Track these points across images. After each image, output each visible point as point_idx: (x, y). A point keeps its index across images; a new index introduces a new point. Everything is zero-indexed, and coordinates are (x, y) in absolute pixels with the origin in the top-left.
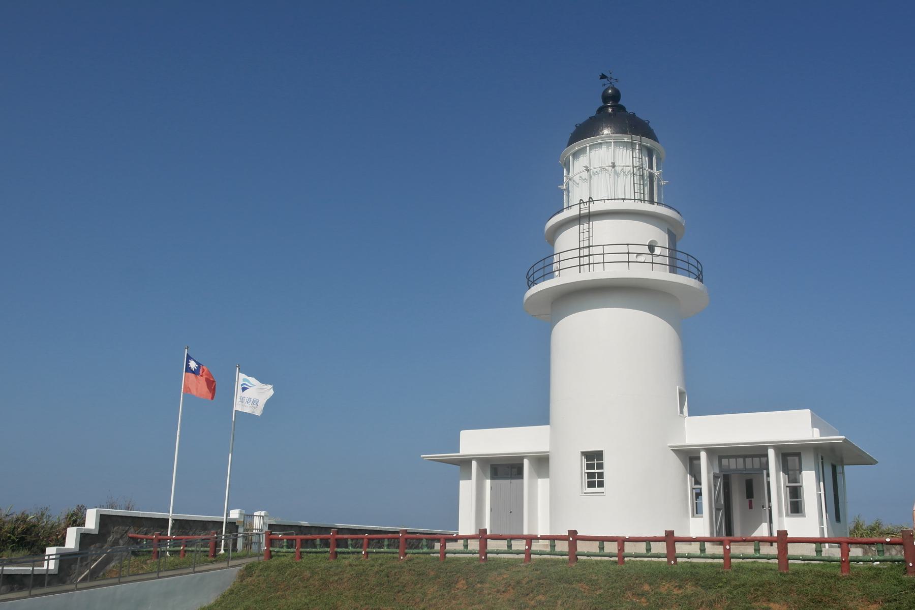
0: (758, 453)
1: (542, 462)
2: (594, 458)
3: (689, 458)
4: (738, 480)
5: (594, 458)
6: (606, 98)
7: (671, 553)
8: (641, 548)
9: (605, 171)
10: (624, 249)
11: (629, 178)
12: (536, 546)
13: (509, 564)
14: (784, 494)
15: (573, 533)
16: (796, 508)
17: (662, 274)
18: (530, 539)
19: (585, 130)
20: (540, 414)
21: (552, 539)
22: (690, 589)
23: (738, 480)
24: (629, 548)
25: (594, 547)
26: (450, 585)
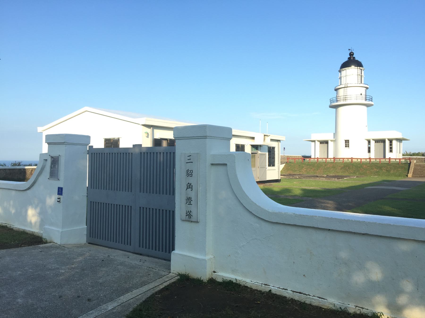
2: (347, 142)
5: (347, 142)
7: (318, 161)
12: (345, 160)
19: (345, 65)
24: (345, 160)
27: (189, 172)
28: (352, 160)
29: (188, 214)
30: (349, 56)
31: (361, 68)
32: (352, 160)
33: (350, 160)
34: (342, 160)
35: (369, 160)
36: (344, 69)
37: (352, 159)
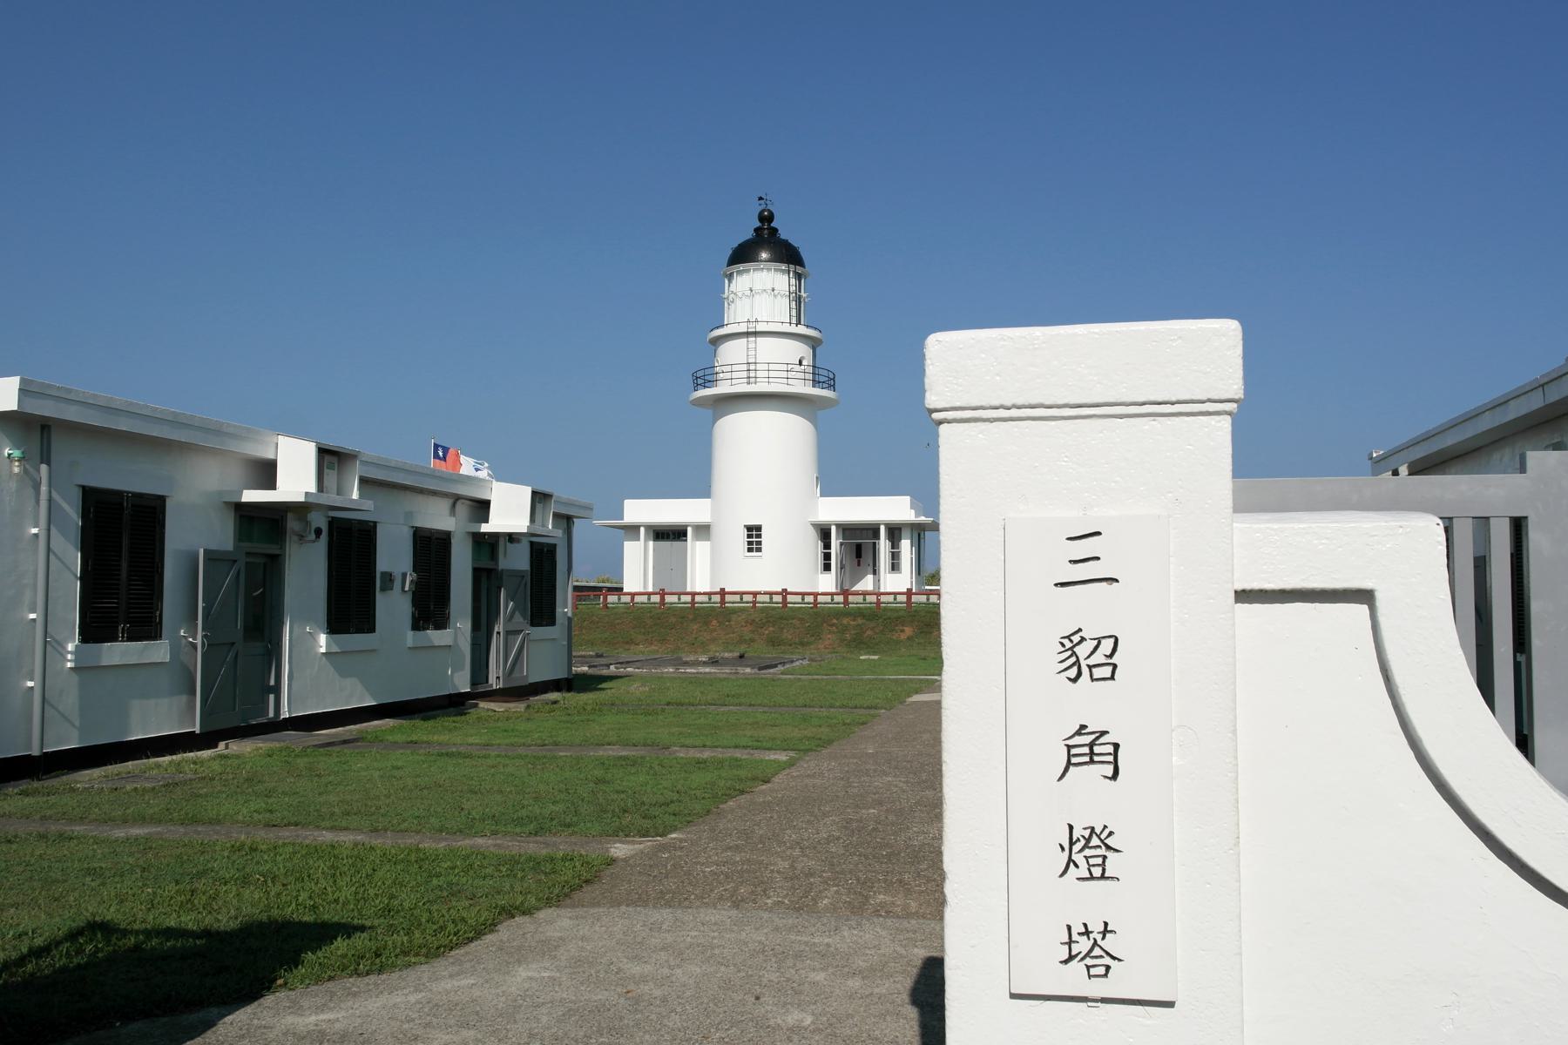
0: (872, 530)
1: (703, 530)
2: (754, 531)
4: (858, 545)
5: (754, 531)
6: (762, 218)
7: (723, 601)
8: (767, 598)
9: (761, 294)
10: (784, 367)
12: (760, 598)
13: (742, 610)
14: (888, 556)
15: (723, 589)
16: (895, 567)
17: (809, 390)
18: (694, 594)
19: (743, 255)
20: (700, 486)
21: (709, 594)
22: (860, 621)
24: (760, 598)
25: (798, 599)
26: (707, 623)
27: (1082, 651)
28: (784, 598)
29: (1083, 945)
30: (758, 224)
31: (799, 269)
32: (784, 598)
33: (778, 598)
35: (840, 599)
36: (741, 267)
37: (785, 593)
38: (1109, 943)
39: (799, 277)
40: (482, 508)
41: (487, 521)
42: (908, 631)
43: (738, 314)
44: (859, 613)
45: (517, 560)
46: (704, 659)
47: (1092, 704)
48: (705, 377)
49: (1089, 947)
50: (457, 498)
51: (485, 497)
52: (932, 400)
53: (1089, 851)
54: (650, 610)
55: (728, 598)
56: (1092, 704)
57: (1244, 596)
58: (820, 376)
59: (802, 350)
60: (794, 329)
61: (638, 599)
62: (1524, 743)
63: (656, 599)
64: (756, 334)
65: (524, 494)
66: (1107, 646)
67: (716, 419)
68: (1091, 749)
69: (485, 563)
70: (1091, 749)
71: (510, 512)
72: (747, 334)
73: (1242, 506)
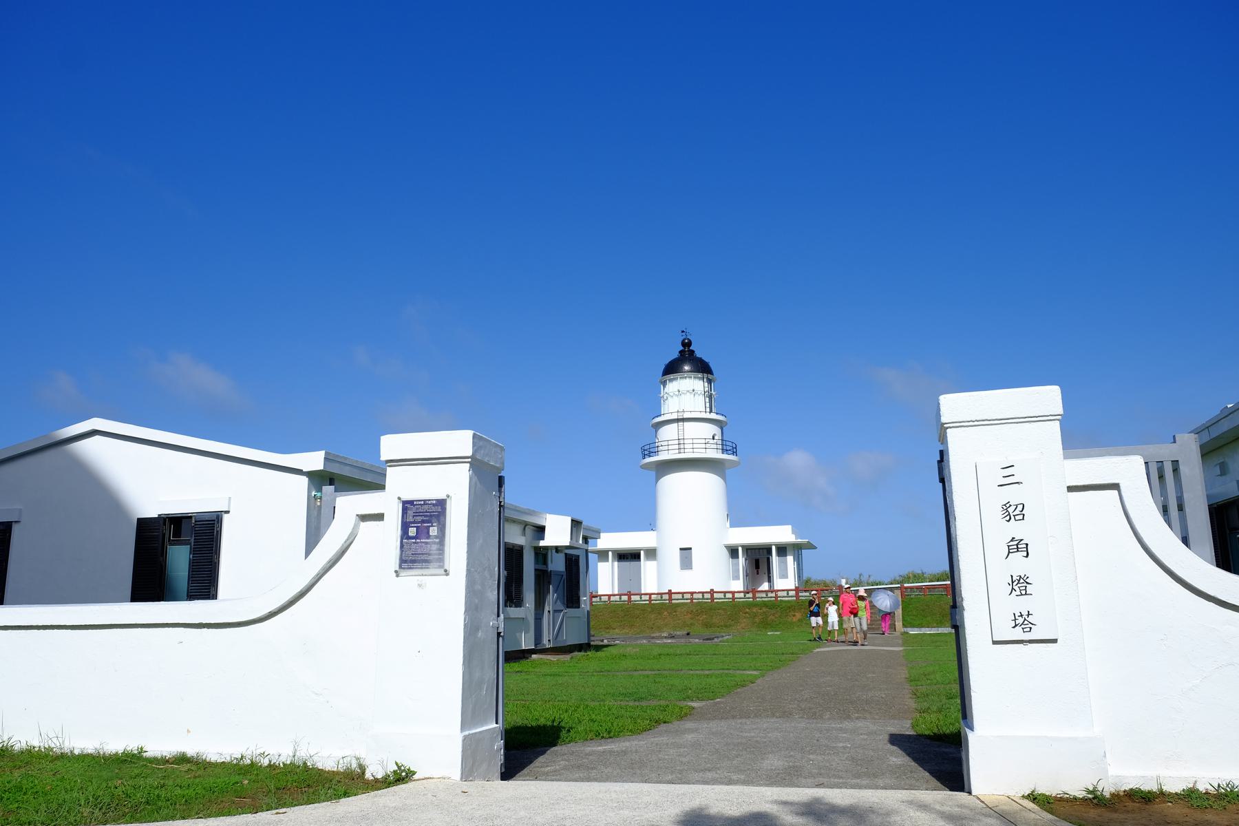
0: (767, 549)
1: (652, 553)
3: (733, 552)
4: (758, 560)
6: (683, 344)
7: (670, 599)
8: (700, 596)
9: (685, 394)
11: (702, 398)
12: (695, 596)
16: (784, 575)
19: (672, 369)
20: (649, 523)
23: (758, 560)
24: (695, 596)
25: (721, 595)
29: (1020, 620)
31: (710, 376)
34: (689, 596)
36: (672, 376)
37: (712, 592)
38: (1030, 619)
39: (710, 382)
40: (540, 530)
41: (543, 539)
42: (798, 615)
43: (670, 408)
44: (765, 604)
45: (557, 564)
46: (665, 634)
47: (1016, 529)
48: (649, 451)
49: (1023, 620)
50: (526, 525)
51: (540, 522)
52: (943, 420)
53: (1020, 584)
54: (621, 606)
55: (674, 596)
56: (1016, 529)
57: (1071, 489)
58: (728, 446)
59: (712, 429)
60: (708, 416)
61: (612, 598)
62: (1185, 541)
63: (625, 598)
64: (683, 420)
65: (567, 521)
66: (1020, 507)
67: (658, 478)
68: (1017, 546)
69: (541, 567)
70: (1017, 546)
71: (558, 533)
72: (678, 420)
73: (1066, 457)
